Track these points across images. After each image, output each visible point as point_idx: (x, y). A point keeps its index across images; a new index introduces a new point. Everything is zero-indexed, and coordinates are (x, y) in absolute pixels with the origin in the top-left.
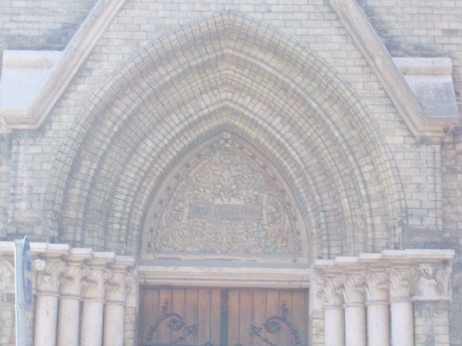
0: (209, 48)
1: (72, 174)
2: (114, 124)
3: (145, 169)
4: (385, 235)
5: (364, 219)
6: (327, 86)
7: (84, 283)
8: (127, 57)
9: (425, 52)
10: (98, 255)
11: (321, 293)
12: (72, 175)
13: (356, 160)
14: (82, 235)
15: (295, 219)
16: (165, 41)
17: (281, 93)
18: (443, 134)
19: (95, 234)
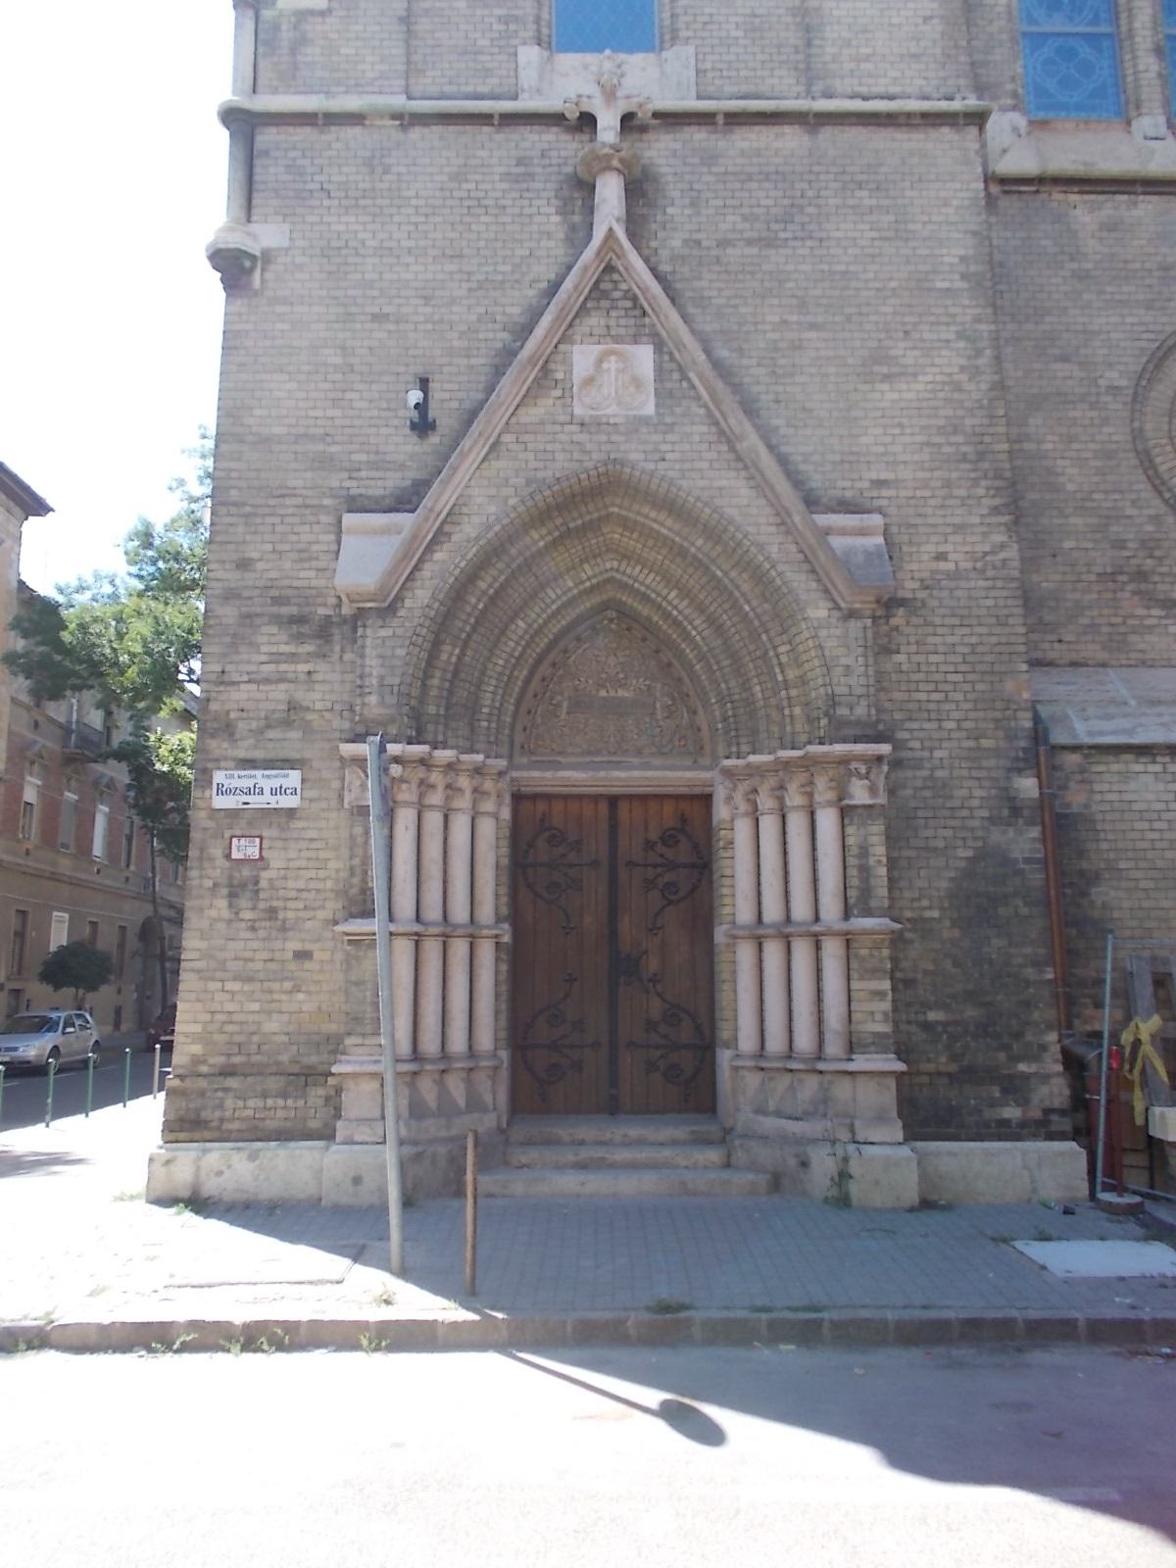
0: (591, 506)
2: (479, 600)
3: (517, 654)
4: (807, 728)
5: (780, 709)
6: (734, 550)
7: (450, 792)
9: (851, 508)
10: (464, 757)
11: (729, 799)
12: (430, 663)
14: (444, 735)
15: (695, 713)
16: (538, 497)
17: (679, 560)
18: (874, 606)
19: (460, 733)
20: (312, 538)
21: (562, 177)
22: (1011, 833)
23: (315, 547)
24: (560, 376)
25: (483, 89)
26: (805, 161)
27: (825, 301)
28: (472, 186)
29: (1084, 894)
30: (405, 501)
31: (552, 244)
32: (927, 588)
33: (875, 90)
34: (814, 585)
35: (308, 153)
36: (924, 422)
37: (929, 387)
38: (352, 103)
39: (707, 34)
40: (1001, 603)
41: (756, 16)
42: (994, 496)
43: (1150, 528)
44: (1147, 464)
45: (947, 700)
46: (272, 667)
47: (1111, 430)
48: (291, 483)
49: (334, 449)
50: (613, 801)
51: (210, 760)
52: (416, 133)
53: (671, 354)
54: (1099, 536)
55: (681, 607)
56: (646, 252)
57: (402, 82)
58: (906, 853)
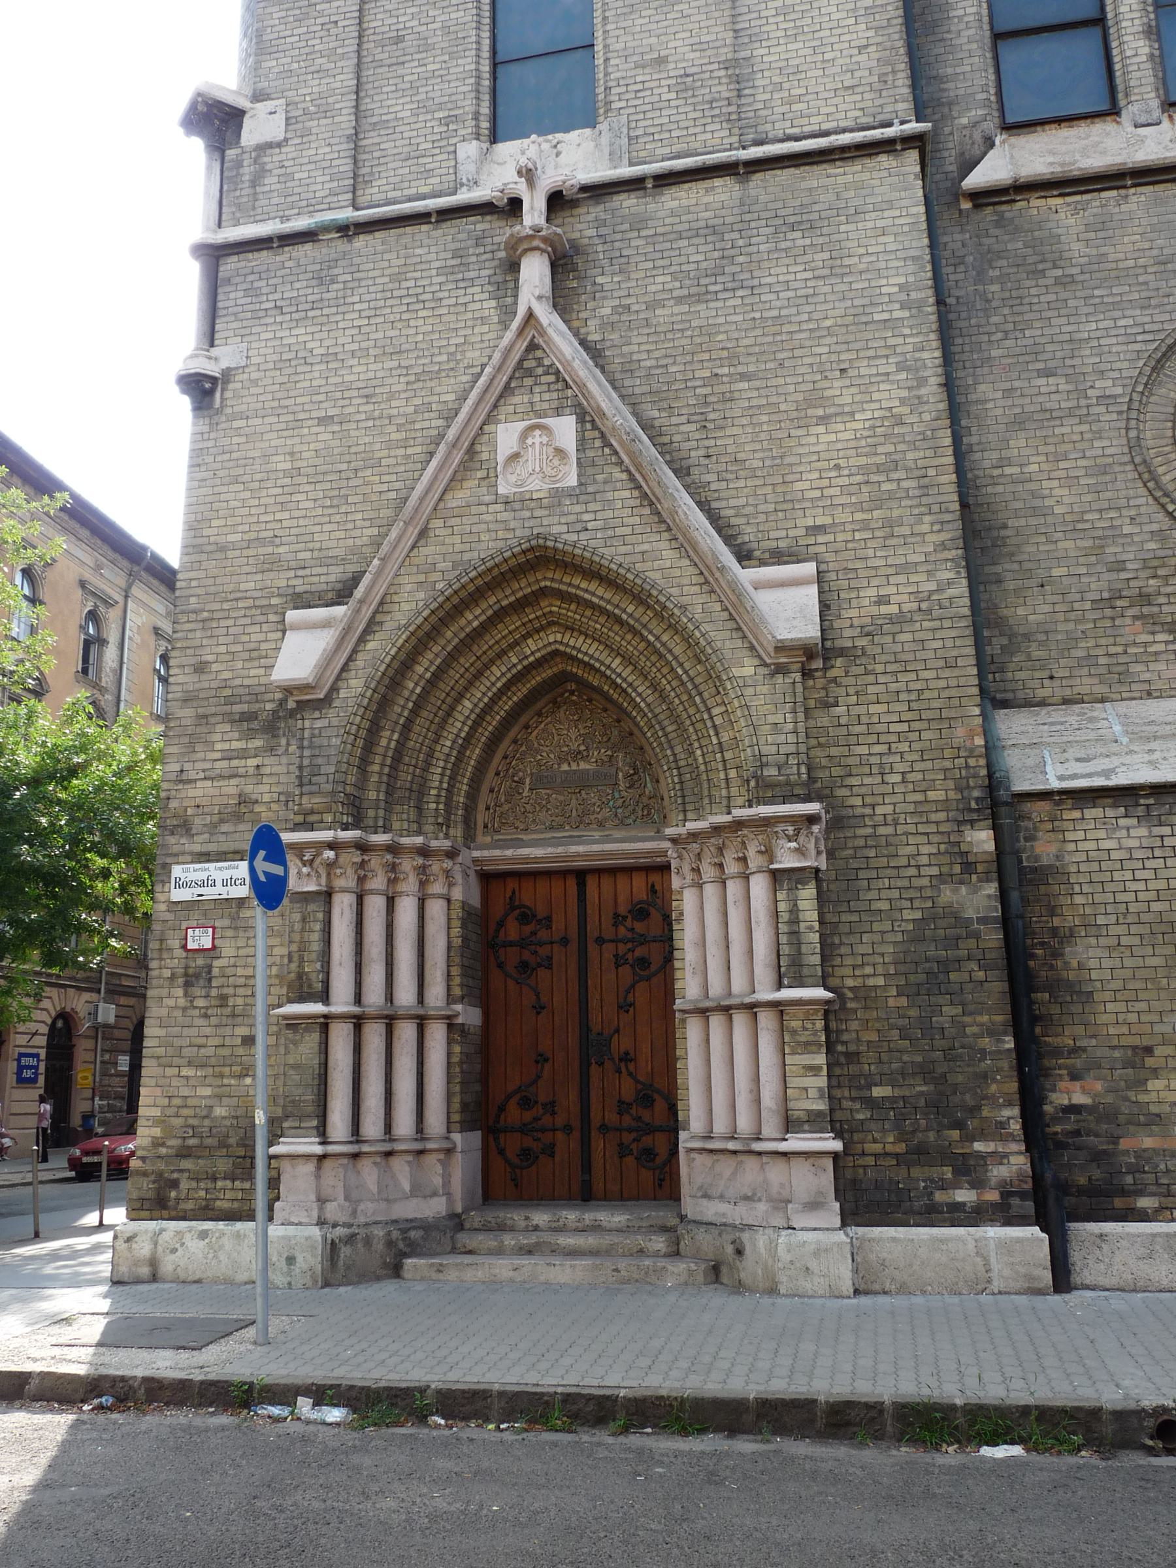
1: (369, 746)
2: (416, 684)
8: (421, 604)
13: (704, 701)
19: (405, 816)
20: (262, 637)
21: (496, 263)
22: (963, 890)
23: (263, 646)
24: (485, 456)
25: (424, 190)
26: (736, 211)
27: (757, 349)
28: (411, 283)
29: (1057, 954)
30: (342, 595)
31: (485, 328)
32: (867, 635)
33: (807, 129)
34: (739, 643)
35: (264, 276)
36: (863, 461)
37: (867, 425)
38: (301, 223)
39: (640, 102)
40: (949, 643)
41: (687, 76)
42: (939, 531)
43: (1152, 545)
44: (1146, 476)
45: (890, 752)
46: (225, 764)
47: (1106, 443)
48: (243, 587)
49: (281, 550)
50: (581, 875)
51: (171, 855)
52: (361, 242)
53: (593, 421)
54: (1093, 559)
55: (624, 675)
56: (576, 324)
57: (350, 196)
58: (845, 917)
